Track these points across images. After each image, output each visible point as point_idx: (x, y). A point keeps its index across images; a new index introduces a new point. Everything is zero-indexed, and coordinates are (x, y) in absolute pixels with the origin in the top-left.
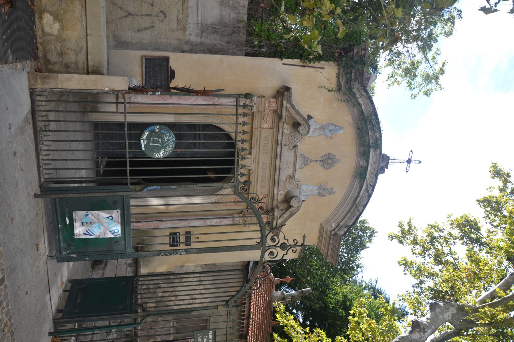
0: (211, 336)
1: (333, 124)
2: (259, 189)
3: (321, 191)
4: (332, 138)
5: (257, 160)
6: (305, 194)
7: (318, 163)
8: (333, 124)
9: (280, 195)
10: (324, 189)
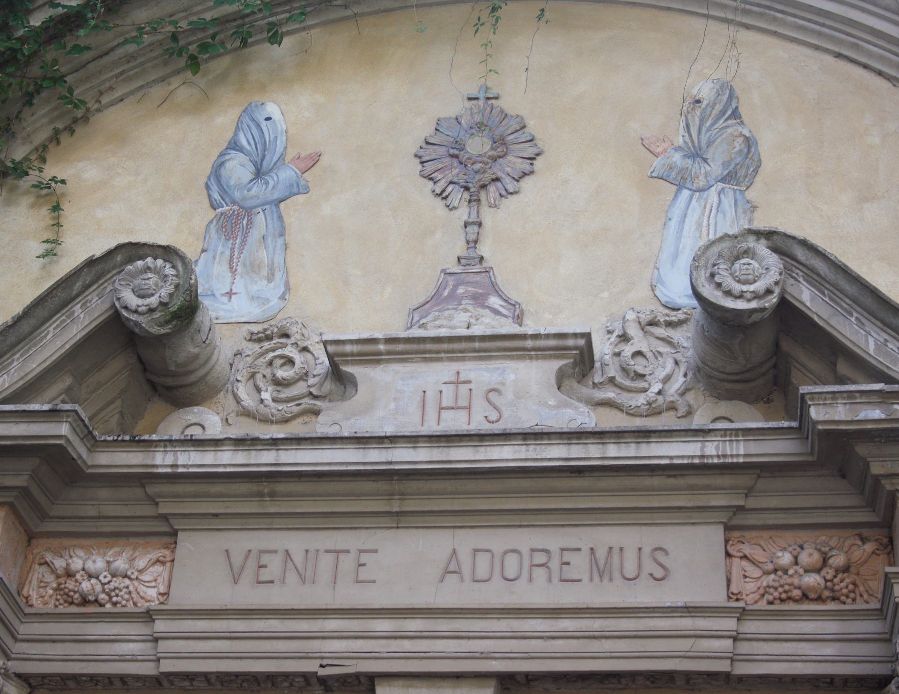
3: (716, 168)
4: (314, 160)
5: (414, 625)
7: (488, 216)
9: (740, 435)
10: (696, 154)
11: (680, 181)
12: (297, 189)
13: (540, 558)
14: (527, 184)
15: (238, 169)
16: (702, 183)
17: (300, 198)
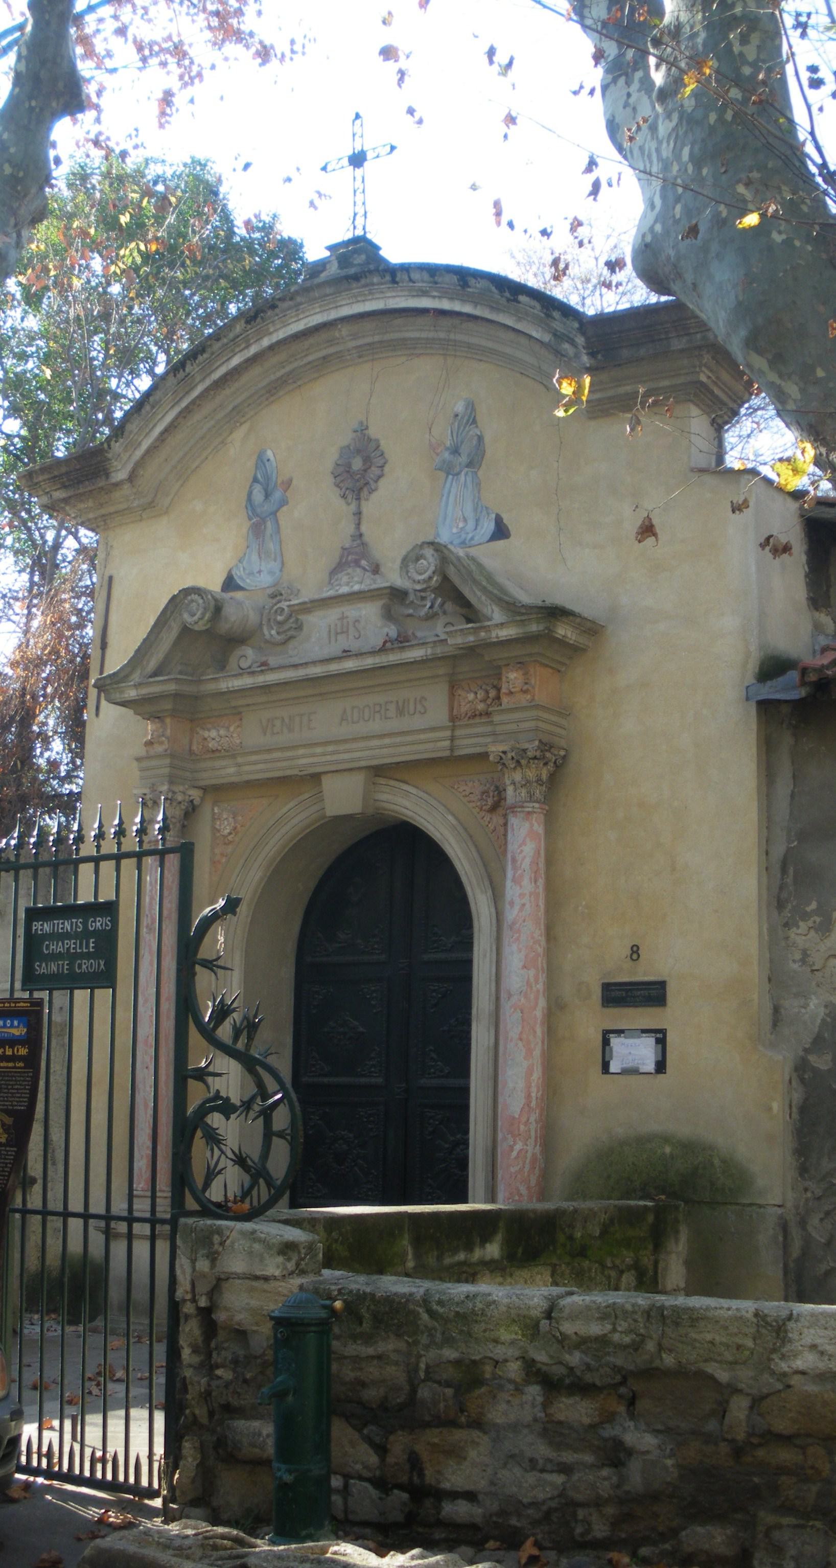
0: (47, 927)
1: (250, 494)
2: (423, 719)
3: (464, 459)
4: (288, 484)
6: (471, 524)
8: (250, 494)
10: (456, 451)
11: (448, 470)
12: (284, 502)
13: (377, 708)
14: (382, 482)
15: (258, 495)
16: (457, 469)
17: (285, 508)
